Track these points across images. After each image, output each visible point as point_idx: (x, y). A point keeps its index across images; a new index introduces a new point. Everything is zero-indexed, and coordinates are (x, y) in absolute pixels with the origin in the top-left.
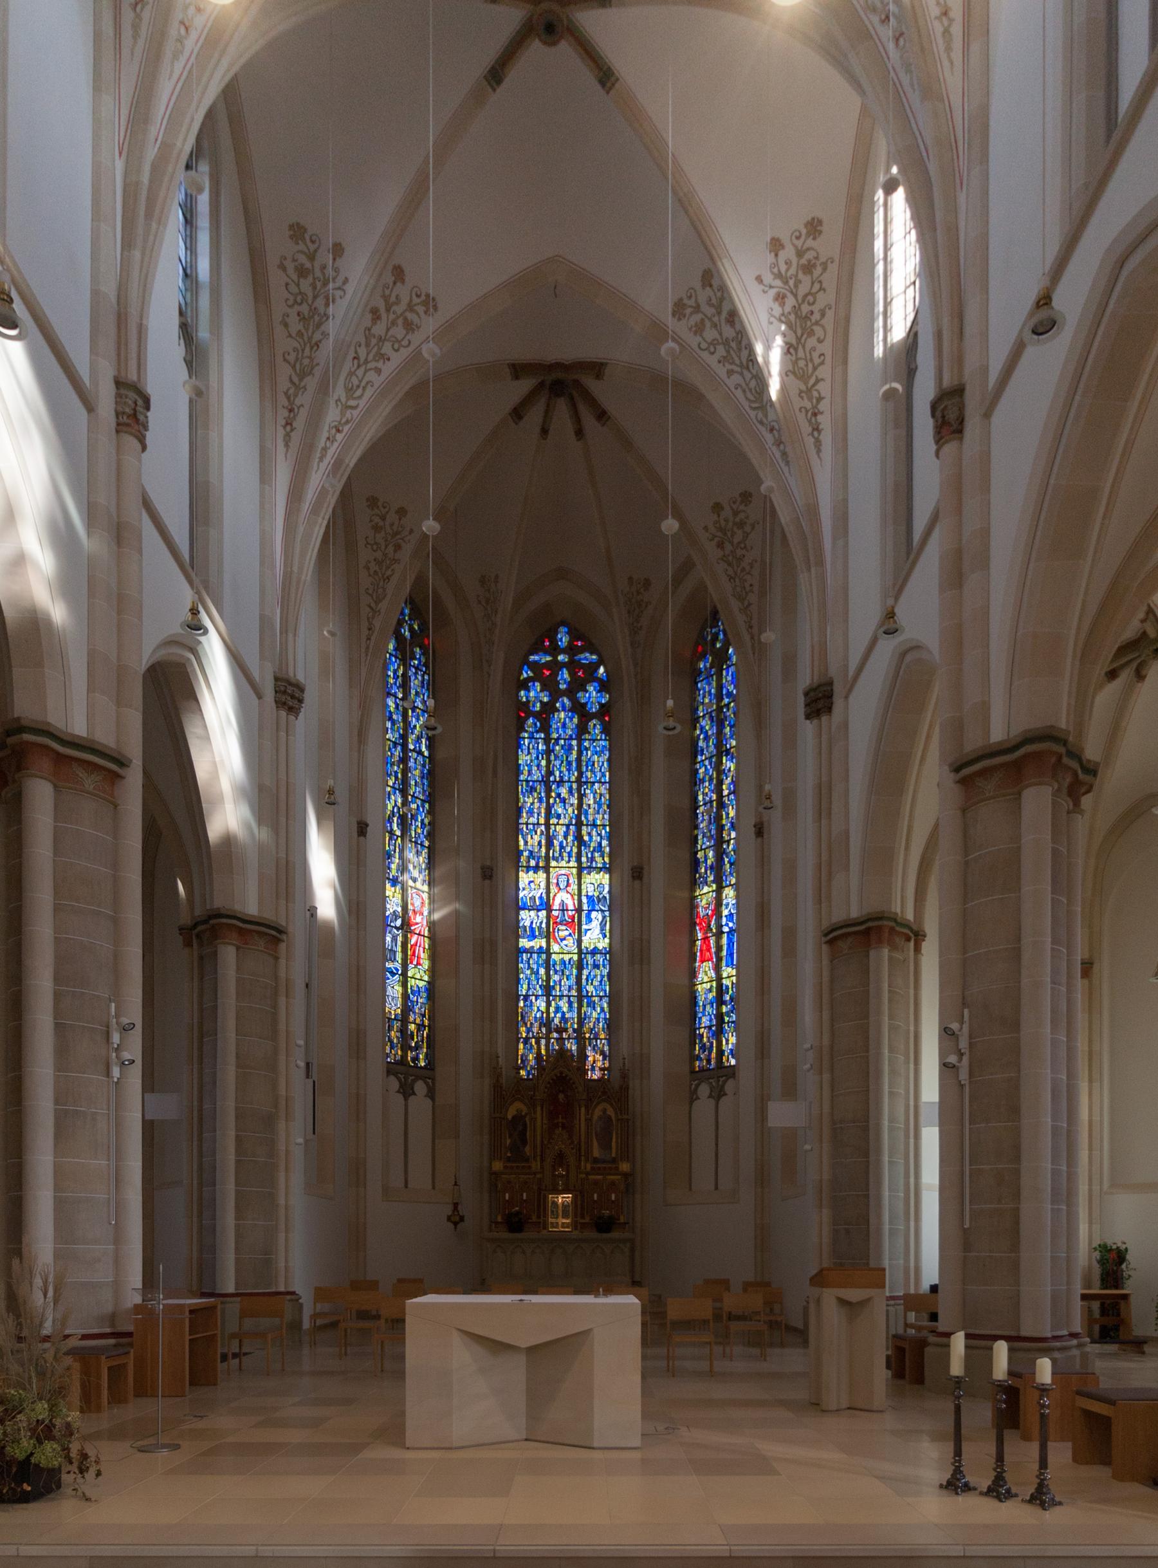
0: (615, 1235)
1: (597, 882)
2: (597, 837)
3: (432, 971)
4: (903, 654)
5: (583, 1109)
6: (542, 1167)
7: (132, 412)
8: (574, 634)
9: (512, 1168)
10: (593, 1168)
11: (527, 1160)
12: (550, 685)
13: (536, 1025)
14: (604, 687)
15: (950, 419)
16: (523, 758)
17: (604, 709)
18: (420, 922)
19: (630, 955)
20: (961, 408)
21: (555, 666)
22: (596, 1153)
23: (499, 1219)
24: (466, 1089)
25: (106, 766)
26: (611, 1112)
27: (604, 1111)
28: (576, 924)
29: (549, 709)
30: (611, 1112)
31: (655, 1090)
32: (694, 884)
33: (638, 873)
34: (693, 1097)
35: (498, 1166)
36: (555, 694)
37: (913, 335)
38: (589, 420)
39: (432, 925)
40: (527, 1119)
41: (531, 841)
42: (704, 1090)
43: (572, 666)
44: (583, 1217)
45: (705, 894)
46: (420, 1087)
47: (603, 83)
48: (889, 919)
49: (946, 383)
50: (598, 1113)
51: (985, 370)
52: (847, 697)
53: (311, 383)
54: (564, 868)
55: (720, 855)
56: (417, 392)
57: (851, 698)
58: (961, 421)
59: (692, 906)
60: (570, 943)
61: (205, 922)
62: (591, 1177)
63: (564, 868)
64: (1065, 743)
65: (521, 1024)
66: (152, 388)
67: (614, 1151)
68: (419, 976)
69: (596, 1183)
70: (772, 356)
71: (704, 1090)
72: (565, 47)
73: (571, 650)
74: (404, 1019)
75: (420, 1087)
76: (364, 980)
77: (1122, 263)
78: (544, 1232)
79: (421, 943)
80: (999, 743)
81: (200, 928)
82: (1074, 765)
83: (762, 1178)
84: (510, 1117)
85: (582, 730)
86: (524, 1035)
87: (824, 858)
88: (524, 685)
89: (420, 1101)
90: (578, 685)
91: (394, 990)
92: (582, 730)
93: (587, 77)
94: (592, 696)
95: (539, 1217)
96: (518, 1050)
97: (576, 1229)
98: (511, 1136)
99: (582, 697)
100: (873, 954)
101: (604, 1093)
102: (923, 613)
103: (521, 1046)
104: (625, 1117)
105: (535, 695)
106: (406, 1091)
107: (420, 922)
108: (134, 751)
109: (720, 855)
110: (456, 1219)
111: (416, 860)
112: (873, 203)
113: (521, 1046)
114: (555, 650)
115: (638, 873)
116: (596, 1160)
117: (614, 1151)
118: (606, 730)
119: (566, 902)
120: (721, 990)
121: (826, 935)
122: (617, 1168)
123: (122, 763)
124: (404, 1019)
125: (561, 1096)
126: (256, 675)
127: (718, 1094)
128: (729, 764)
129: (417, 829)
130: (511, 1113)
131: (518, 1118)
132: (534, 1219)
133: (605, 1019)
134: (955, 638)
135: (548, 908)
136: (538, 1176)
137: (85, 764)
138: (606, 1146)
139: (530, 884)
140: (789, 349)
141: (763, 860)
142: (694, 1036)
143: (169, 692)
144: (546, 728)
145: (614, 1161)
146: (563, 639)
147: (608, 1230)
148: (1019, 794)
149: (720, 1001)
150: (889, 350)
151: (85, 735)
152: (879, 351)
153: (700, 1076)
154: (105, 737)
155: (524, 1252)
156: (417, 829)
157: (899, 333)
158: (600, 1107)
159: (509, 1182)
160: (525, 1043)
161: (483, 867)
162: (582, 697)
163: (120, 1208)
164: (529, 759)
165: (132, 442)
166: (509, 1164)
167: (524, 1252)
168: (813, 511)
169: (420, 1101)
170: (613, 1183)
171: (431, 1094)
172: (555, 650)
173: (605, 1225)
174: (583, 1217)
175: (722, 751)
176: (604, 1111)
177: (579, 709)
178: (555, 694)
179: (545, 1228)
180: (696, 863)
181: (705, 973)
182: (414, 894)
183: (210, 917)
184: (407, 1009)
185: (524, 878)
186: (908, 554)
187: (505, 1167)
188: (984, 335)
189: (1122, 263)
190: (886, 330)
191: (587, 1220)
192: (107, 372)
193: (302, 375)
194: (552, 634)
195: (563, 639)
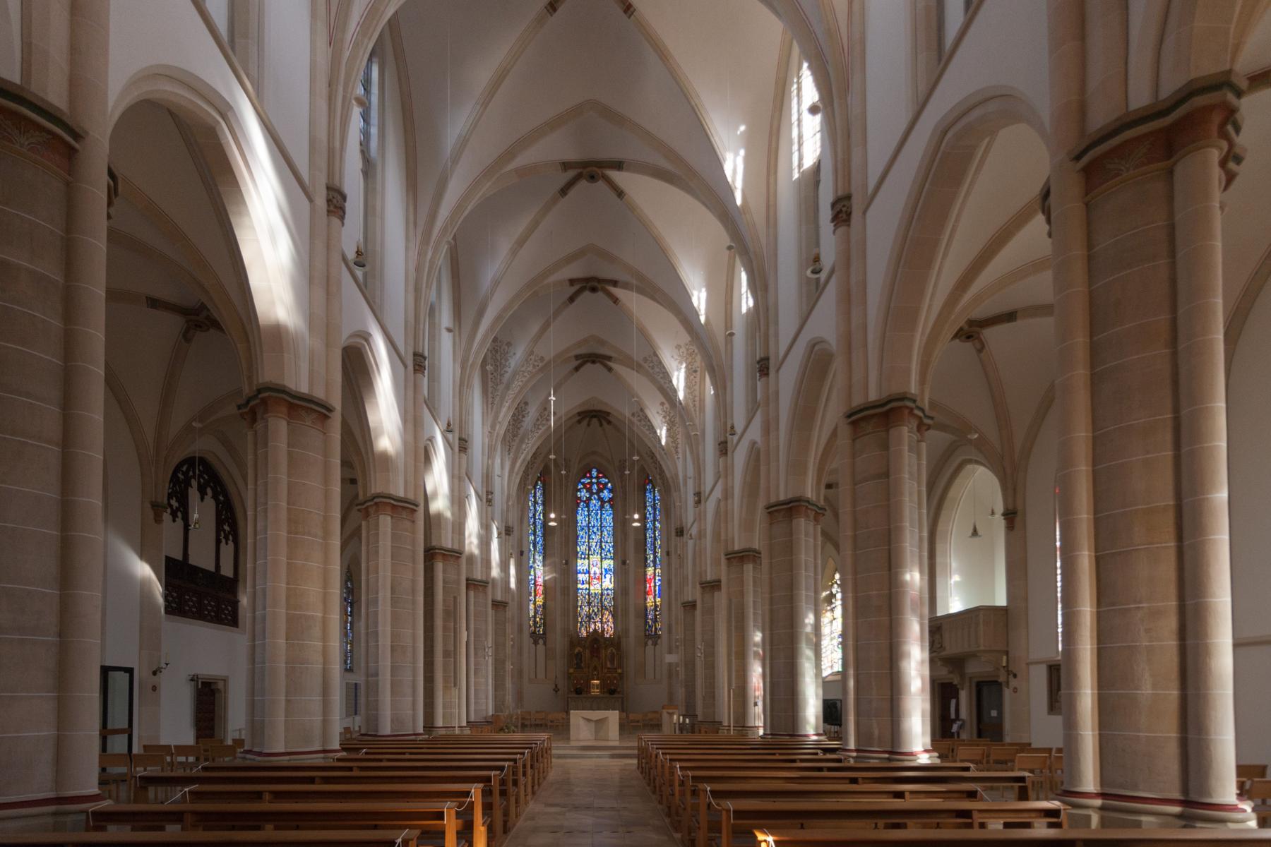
1: (609, 563)
2: (608, 546)
3: (545, 599)
4: (814, 346)
7: (336, 203)
8: (599, 472)
12: (589, 490)
14: (610, 491)
15: (842, 213)
16: (579, 518)
17: (611, 500)
18: (540, 581)
19: (622, 589)
20: (850, 207)
21: (591, 484)
24: (559, 642)
25: (321, 411)
28: (600, 579)
29: (589, 499)
31: (631, 643)
32: (646, 566)
33: (624, 563)
34: (646, 644)
36: (591, 494)
37: (817, 168)
38: (604, 423)
39: (545, 582)
41: (582, 548)
42: (650, 642)
43: (598, 483)
45: (650, 571)
46: (541, 641)
47: (625, 12)
48: (910, 399)
49: (840, 193)
51: (865, 186)
52: (865, 213)
53: (517, 439)
54: (595, 559)
55: (655, 557)
56: (548, 439)
57: (869, 214)
58: (849, 214)
59: (645, 574)
60: (598, 586)
61: (255, 397)
63: (595, 559)
64: (915, 401)
66: (347, 189)
68: (540, 600)
70: (663, 433)
71: (650, 642)
72: (601, 184)
73: (598, 478)
74: (535, 617)
75: (541, 641)
76: (522, 607)
77: (945, 132)
79: (540, 589)
80: (1144, 108)
81: (252, 403)
82: (920, 414)
83: (670, 677)
85: (602, 507)
88: (579, 490)
89: (541, 647)
90: (600, 491)
91: (532, 606)
92: (602, 507)
93: (613, 196)
94: (606, 494)
99: (602, 495)
100: (795, 521)
102: (825, 324)
105: (584, 494)
106: (536, 643)
107: (540, 581)
108: (336, 401)
109: (655, 557)
110: (556, 690)
111: (539, 558)
112: (790, 92)
114: (591, 477)
115: (624, 563)
118: (611, 507)
119: (596, 573)
120: (656, 606)
121: (1078, 158)
123: (330, 410)
124: (535, 617)
126: (402, 348)
127: (655, 644)
128: (658, 525)
129: (539, 547)
134: (847, 340)
135: (589, 572)
137: (304, 408)
139: (582, 564)
140: (668, 430)
141: (669, 565)
142: (646, 623)
143: (356, 369)
144: (588, 506)
146: (594, 473)
148: (1171, 172)
149: (655, 610)
150: (803, 174)
151: (18, 81)
152: (796, 175)
153: (648, 637)
154: (319, 394)
156: (539, 547)
157: (809, 162)
161: (562, 549)
162: (602, 495)
163: (487, 690)
164: (581, 518)
165: (336, 221)
168: (677, 475)
169: (541, 647)
171: (545, 643)
172: (591, 477)
173: (612, 692)
175: (655, 520)
177: (601, 499)
178: (591, 494)
180: (646, 559)
181: (650, 599)
182: (540, 572)
183: (259, 391)
184: (536, 613)
185: (580, 562)
186: (940, 60)
188: (777, 335)
189: (945, 132)
190: (801, 159)
192: (322, 180)
193: (514, 436)
194: (590, 472)
195: (594, 473)
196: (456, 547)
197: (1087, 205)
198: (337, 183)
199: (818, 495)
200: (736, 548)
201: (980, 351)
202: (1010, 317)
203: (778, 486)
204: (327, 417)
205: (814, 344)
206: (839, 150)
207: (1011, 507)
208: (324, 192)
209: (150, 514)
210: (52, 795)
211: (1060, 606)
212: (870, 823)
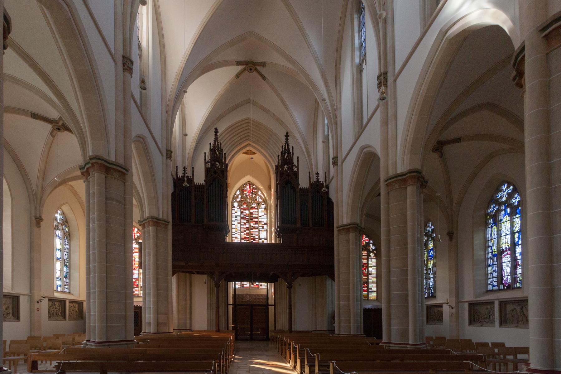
66: (133, 59)
121: (386, 181)
154: (165, 218)
165: (128, 74)
196: (121, 162)
197: (388, 193)
198: (128, 55)
199: (361, 222)
200: (345, 223)
201: (441, 157)
202: (457, 140)
203: (343, 218)
204: (167, 225)
205: (363, 148)
206: (382, 53)
207: (451, 231)
208: (121, 58)
209: (34, 222)
210: (106, 340)
211: (75, 361)
212: (221, 309)
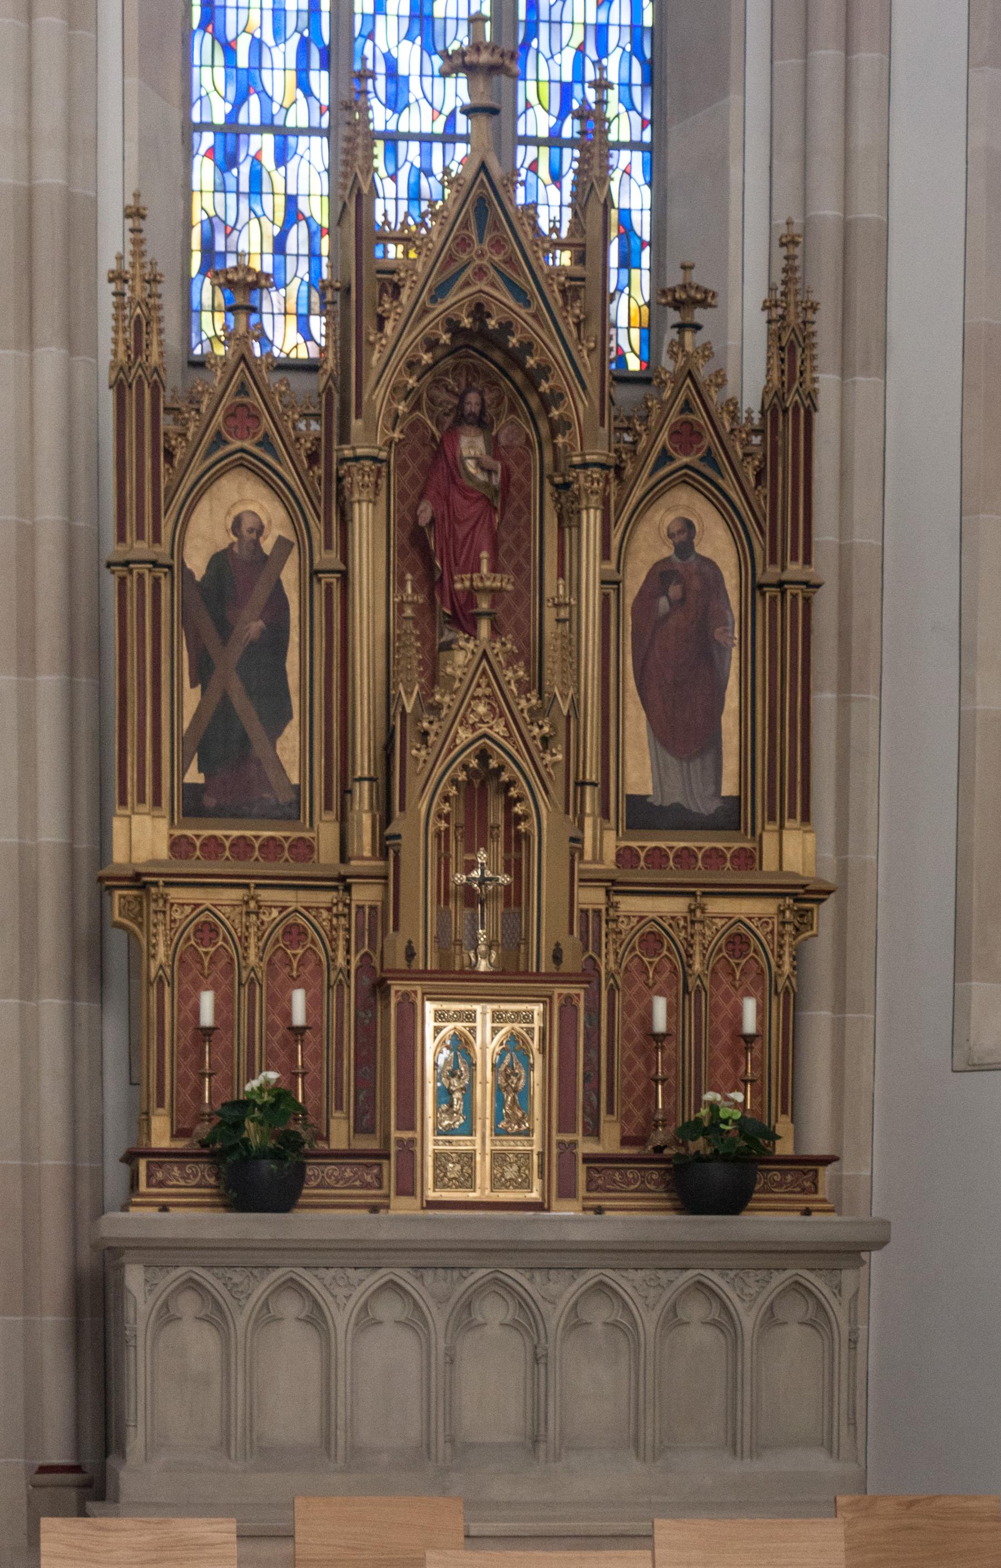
0: (765, 1222)
5: (591, 520)
6: (386, 845)
9: (212, 847)
10: (626, 857)
11: (291, 811)
13: (282, 56)
22: (639, 775)
23: (161, 1134)
26: (717, 544)
27: (685, 535)
30: (717, 544)
35: (143, 837)
40: (289, 576)
44: (593, 1131)
50: (649, 547)
62: (629, 905)
65: (203, 45)
67: (730, 765)
69: (652, 937)
78: (403, 1207)
84: (197, 563)
86: (219, 112)
87: (49, 117)
95: (362, 1126)
96: (187, 192)
97: (567, 1192)
98: (201, 675)
101: (686, 435)
103: (204, 172)
104: (795, 570)
113: (204, 172)
116: (641, 814)
117: (730, 765)
122: (749, 859)
125: (471, 446)
130: (204, 538)
131: (239, 569)
132: (340, 1134)
133: (636, 28)
136: (365, 895)
138: (685, 730)
145: (731, 817)
147: (733, 1201)
155: (316, 1318)
158: (662, 517)
159: (207, 931)
160: (227, 160)
166: (198, 832)
167: (316, 1318)
170: (738, 941)
174: (593, 1131)
176: (685, 535)
179: (407, 1187)
187: (178, 846)
191: (609, 1141)
